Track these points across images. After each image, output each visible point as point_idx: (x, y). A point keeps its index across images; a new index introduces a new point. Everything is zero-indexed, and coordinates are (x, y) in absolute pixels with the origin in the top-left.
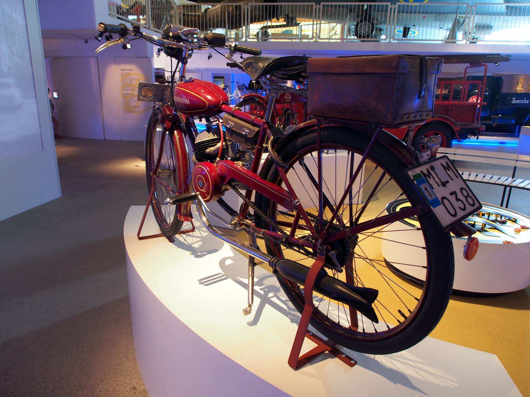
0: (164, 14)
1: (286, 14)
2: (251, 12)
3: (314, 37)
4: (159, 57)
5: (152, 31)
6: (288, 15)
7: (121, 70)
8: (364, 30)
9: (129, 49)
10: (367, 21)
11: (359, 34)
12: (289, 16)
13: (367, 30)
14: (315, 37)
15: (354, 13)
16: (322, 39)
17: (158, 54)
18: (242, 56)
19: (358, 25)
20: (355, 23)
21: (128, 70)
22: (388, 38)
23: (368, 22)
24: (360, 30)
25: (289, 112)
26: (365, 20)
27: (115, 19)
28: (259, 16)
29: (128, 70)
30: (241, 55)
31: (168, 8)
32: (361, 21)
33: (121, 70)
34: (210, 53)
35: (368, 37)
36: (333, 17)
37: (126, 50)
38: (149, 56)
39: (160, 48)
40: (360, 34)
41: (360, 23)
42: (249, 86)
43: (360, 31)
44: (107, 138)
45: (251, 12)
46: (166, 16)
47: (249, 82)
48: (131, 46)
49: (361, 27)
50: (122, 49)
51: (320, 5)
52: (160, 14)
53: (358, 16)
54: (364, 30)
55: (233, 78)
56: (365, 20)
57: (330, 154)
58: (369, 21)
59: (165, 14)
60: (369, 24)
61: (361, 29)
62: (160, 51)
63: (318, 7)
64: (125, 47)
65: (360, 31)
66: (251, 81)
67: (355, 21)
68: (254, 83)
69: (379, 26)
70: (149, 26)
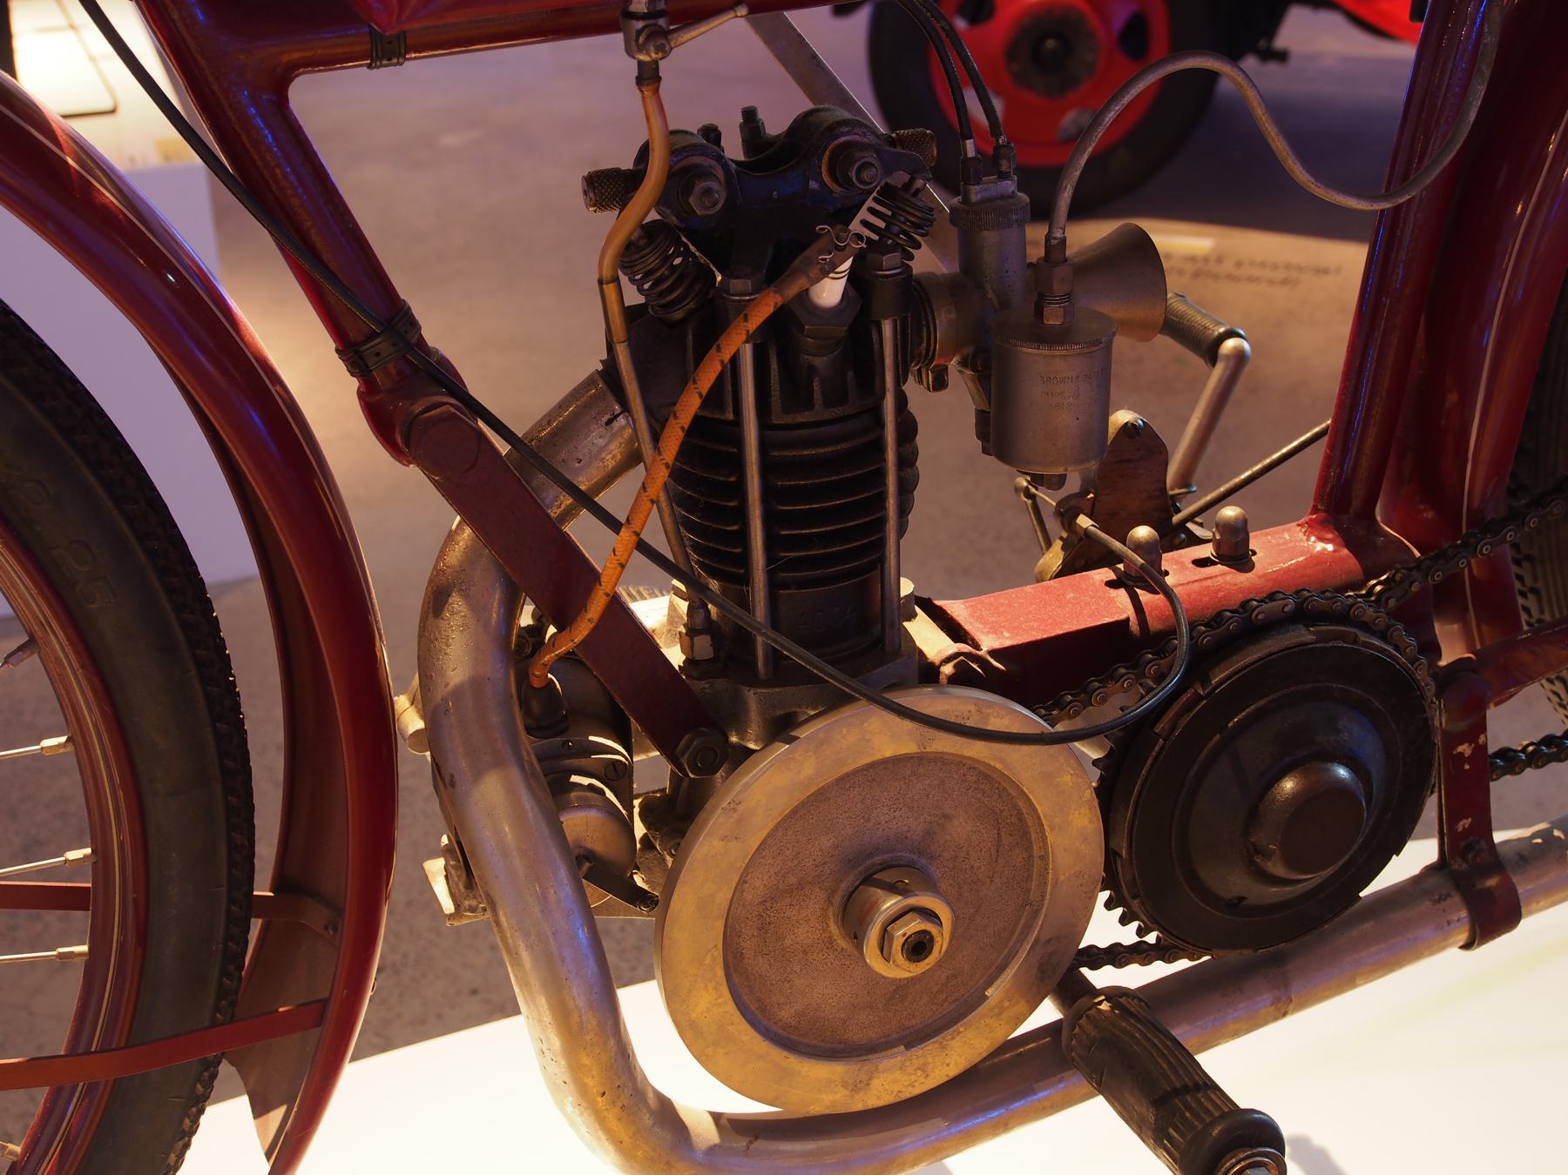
25: (830, 292)
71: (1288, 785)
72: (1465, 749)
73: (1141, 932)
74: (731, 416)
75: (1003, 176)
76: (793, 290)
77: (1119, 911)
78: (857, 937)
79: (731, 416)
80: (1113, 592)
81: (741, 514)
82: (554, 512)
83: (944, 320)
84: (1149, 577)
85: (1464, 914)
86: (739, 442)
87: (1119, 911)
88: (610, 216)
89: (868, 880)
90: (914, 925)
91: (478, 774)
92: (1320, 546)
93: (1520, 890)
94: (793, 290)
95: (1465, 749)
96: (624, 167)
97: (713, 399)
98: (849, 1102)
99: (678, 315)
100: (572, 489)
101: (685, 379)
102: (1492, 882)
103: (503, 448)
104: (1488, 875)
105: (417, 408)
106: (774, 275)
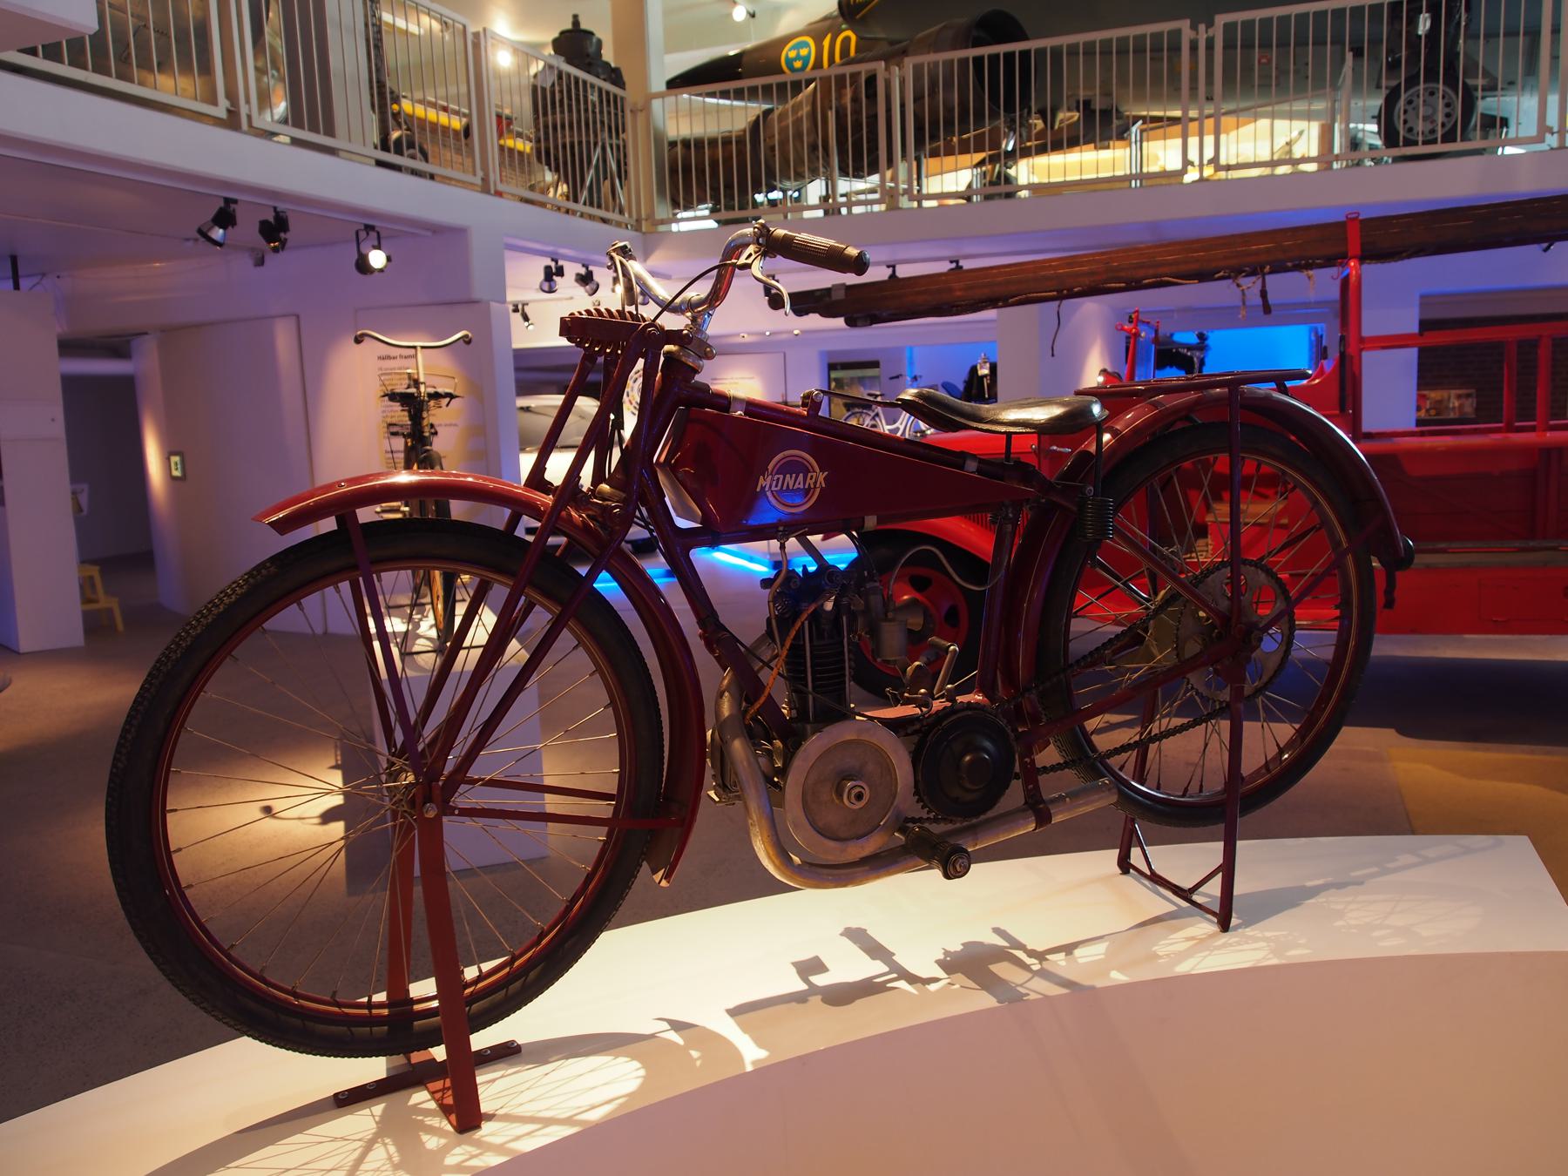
0: (588, 143)
1: (1078, 102)
2: (915, 100)
3: (1192, 164)
4: (260, 262)
5: (1127, 343)
6: (1087, 103)
7: (379, 358)
8: (1425, 119)
9: (381, 270)
10: (1438, 82)
11: (1404, 137)
12: (1092, 107)
13: (1440, 118)
14: (1197, 163)
15: (1375, 57)
16: (1228, 168)
17: (546, 289)
18: (894, 271)
19: (1399, 97)
20: (1376, 102)
21: (405, 357)
22: (1553, 134)
23: (1444, 83)
24: (1405, 122)
25: (829, 606)
26: (1431, 75)
27: (368, 168)
28: (949, 110)
29: (405, 357)
30: (891, 269)
31: (610, 119)
32: (1412, 81)
33: (379, 358)
34: (772, 273)
35: (1449, 137)
36: (1274, 87)
37: (368, 278)
38: (478, 293)
39: (553, 264)
40: (1408, 136)
41: (1405, 92)
42: (965, 388)
43: (1408, 126)
44: (331, 630)
45: (918, 98)
46: (599, 150)
47: (964, 375)
48: (389, 259)
49: (1409, 108)
50: (354, 268)
51: (1210, 24)
52: (580, 143)
53: (1393, 66)
54: (1429, 119)
55: (912, 364)
56: (1431, 75)
57: (1273, 904)
58: (1451, 81)
59: (596, 144)
60: (1449, 91)
61: (1410, 116)
62: (555, 277)
63: (1205, 36)
64: (363, 266)
65: (1408, 126)
66: (974, 370)
67: (1379, 87)
68: (985, 376)
69: (1486, 105)
70: (485, 180)
71: (968, 758)
72: (1027, 760)
73: (928, 813)
74: (802, 643)
75: (875, 581)
76: (819, 603)
77: (917, 797)
78: (840, 796)
79: (802, 643)
80: (570, 20)
81: (805, 672)
82: (756, 668)
83: (860, 621)
84: (927, 705)
85: (1033, 818)
86: (805, 651)
87: (917, 797)
88: (768, 591)
89: (843, 780)
90: (858, 789)
91: (733, 739)
92: (979, 698)
93: (1052, 812)
94: (819, 603)
95: (1027, 760)
96: (415, 1053)
97: (796, 637)
98: (827, 588)
99: (787, 616)
100: (762, 661)
101: (788, 635)
102: (1041, 806)
103: (743, 649)
104: (1041, 804)
105: (720, 635)
106: (814, 600)
